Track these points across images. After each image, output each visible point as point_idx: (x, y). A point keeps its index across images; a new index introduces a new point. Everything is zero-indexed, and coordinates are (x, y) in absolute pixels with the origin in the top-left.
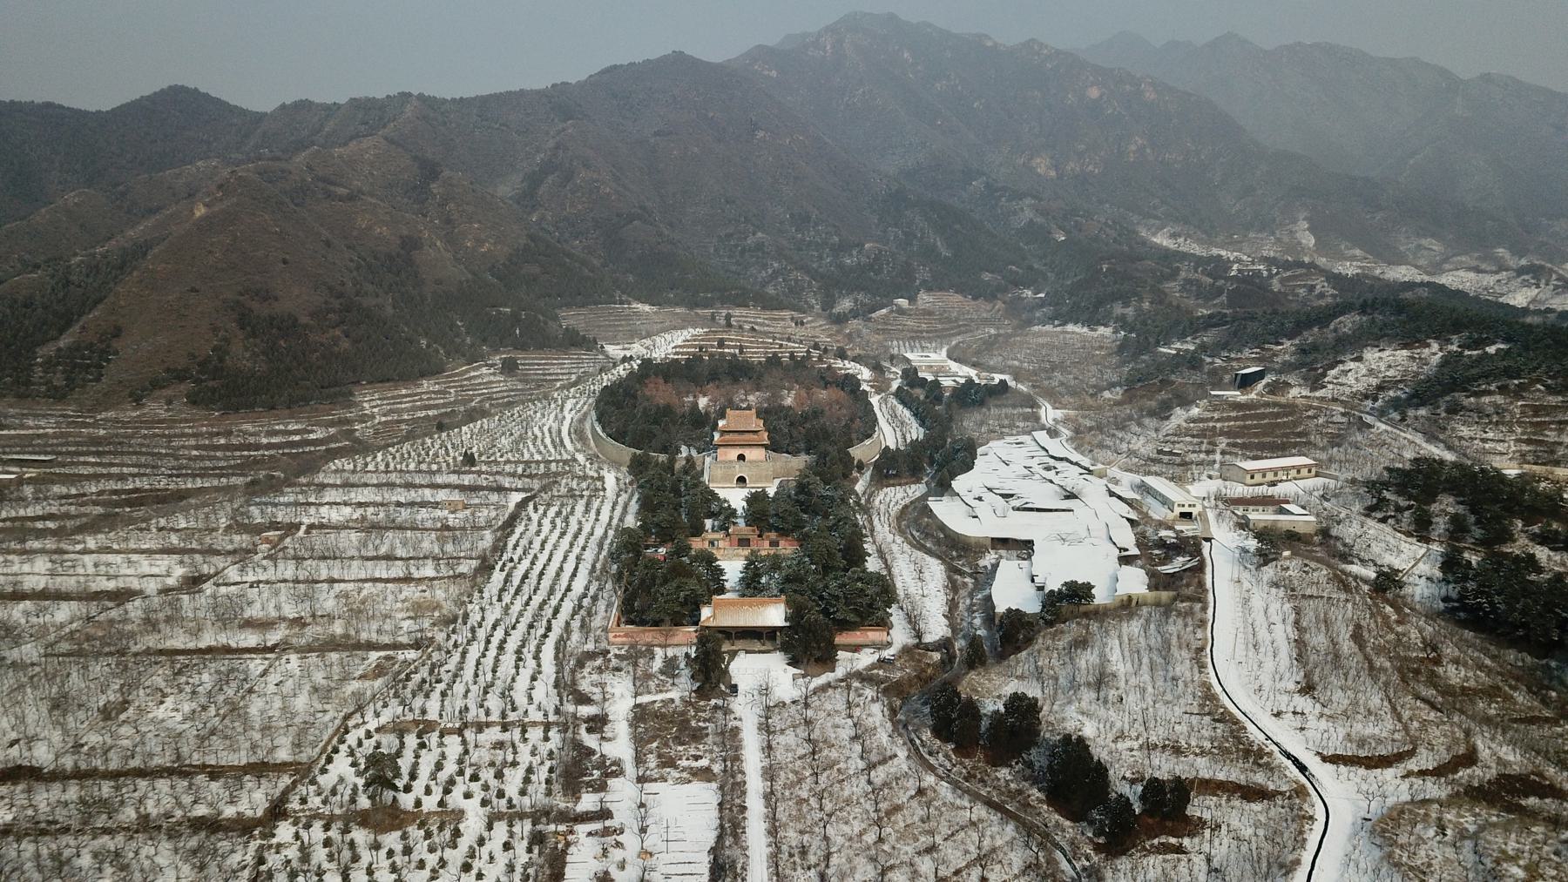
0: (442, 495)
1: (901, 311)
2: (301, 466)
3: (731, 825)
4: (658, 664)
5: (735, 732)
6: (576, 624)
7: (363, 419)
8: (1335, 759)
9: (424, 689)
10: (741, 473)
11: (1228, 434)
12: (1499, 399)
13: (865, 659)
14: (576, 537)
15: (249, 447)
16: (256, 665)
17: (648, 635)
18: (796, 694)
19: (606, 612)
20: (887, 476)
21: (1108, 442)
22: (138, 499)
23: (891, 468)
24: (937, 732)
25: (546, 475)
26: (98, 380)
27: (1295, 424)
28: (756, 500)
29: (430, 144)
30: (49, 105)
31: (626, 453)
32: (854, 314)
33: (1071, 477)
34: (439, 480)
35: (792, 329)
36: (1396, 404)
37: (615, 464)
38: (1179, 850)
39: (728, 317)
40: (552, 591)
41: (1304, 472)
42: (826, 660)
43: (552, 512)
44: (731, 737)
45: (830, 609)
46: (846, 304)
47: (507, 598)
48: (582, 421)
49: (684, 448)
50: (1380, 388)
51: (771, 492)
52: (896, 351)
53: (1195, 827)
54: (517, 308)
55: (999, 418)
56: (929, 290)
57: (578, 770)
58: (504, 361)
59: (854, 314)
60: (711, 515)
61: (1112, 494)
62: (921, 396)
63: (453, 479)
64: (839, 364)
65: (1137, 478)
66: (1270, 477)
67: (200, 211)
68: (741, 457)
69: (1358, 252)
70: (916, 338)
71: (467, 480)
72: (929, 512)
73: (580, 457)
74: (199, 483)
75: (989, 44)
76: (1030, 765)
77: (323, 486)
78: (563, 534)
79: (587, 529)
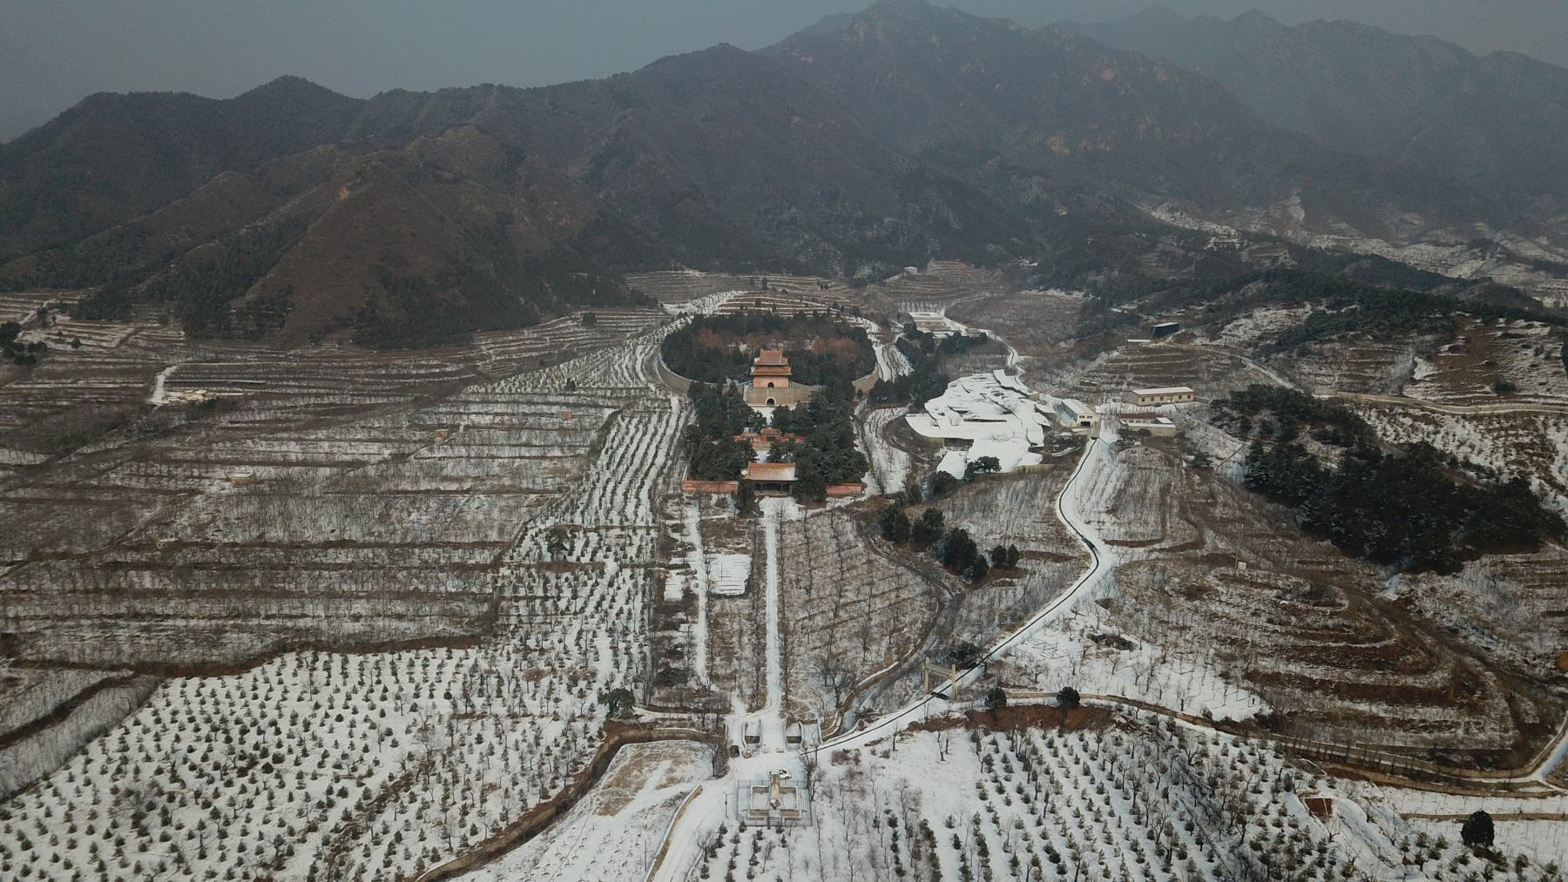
0: (555, 409)
1: (911, 277)
2: (446, 391)
3: (758, 569)
4: (713, 502)
5: (762, 534)
6: (660, 481)
7: (483, 357)
8: (1112, 543)
9: (573, 507)
10: (768, 395)
11: (1132, 370)
12: (1337, 346)
13: (846, 502)
14: (654, 435)
15: (403, 376)
16: (462, 500)
17: (707, 486)
18: (801, 515)
19: (682, 470)
20: (880, 401)
21: (1048, 376)
22: (340, 410)
23: (883, 394)
24: (884, 536)
25: (627, 398)
26: (281, 326)
27: (1190, 365)
28: (780, 413)
29: (515, 129)
30: (186, 95)
31: (686, 383)
32: (872, 279)
33: (1012, 399)
34: (551, 399)
35: (818, 291)
36: (1268, 351)
37: (678, 391)
38: (1011, 584)
39: (765, 282)
40: (642, 464)
41: (1185, 397)
42: (821, 502)
43: (635, 421)
44: (759, 536)
45: (825, 463)
46: (866, 271)
47: (613, 468)
48: (651, 360)
49: (729, 381)
50: (1261, 338)
51: (792, 408)
52: (902, 311)
53: (1021, 573)
54: (593, 273)
55: (973, 362)
56: (938, 259)
57: (667, 547)
58: (585, 316)
59: (872, 279)
60: (748, 424)
61: (1037, 410)
62: (918, 345)
63: (561, 399)
64: (853, 320)
65: (1059, 401)
66: (1157, 400)
67: (345, 194)
68: (771, 385)
69: (1343, 226)
70: (922, 300)
71: (571, 400)
72: (905, 423)
73: (652, 387)
74: (373, 401)
75: (1013, 28)
76: (936, 549)
77: (467, 403)
78: (644, 434)
79: (661, 431)
